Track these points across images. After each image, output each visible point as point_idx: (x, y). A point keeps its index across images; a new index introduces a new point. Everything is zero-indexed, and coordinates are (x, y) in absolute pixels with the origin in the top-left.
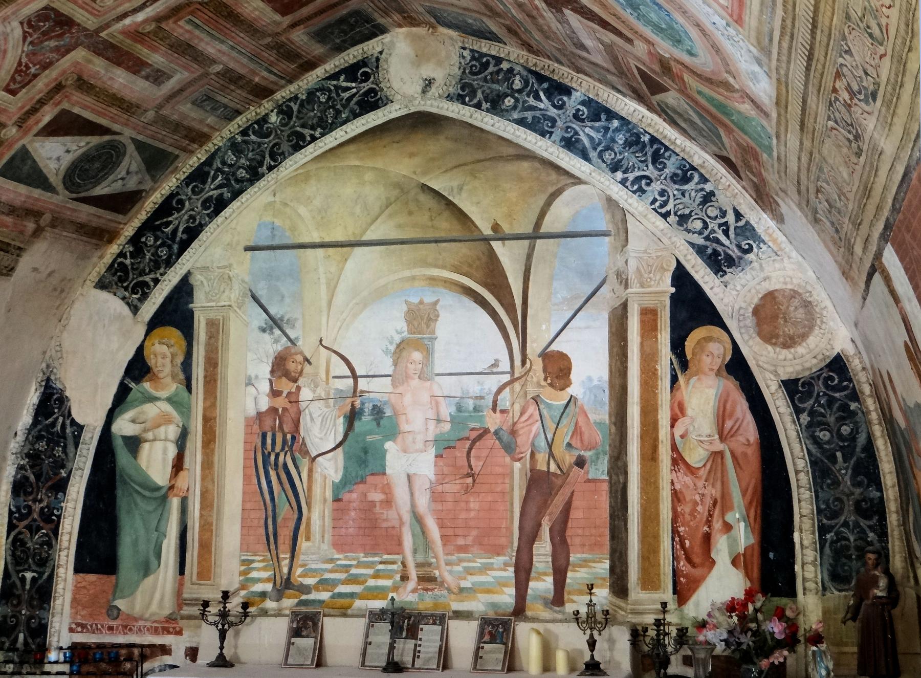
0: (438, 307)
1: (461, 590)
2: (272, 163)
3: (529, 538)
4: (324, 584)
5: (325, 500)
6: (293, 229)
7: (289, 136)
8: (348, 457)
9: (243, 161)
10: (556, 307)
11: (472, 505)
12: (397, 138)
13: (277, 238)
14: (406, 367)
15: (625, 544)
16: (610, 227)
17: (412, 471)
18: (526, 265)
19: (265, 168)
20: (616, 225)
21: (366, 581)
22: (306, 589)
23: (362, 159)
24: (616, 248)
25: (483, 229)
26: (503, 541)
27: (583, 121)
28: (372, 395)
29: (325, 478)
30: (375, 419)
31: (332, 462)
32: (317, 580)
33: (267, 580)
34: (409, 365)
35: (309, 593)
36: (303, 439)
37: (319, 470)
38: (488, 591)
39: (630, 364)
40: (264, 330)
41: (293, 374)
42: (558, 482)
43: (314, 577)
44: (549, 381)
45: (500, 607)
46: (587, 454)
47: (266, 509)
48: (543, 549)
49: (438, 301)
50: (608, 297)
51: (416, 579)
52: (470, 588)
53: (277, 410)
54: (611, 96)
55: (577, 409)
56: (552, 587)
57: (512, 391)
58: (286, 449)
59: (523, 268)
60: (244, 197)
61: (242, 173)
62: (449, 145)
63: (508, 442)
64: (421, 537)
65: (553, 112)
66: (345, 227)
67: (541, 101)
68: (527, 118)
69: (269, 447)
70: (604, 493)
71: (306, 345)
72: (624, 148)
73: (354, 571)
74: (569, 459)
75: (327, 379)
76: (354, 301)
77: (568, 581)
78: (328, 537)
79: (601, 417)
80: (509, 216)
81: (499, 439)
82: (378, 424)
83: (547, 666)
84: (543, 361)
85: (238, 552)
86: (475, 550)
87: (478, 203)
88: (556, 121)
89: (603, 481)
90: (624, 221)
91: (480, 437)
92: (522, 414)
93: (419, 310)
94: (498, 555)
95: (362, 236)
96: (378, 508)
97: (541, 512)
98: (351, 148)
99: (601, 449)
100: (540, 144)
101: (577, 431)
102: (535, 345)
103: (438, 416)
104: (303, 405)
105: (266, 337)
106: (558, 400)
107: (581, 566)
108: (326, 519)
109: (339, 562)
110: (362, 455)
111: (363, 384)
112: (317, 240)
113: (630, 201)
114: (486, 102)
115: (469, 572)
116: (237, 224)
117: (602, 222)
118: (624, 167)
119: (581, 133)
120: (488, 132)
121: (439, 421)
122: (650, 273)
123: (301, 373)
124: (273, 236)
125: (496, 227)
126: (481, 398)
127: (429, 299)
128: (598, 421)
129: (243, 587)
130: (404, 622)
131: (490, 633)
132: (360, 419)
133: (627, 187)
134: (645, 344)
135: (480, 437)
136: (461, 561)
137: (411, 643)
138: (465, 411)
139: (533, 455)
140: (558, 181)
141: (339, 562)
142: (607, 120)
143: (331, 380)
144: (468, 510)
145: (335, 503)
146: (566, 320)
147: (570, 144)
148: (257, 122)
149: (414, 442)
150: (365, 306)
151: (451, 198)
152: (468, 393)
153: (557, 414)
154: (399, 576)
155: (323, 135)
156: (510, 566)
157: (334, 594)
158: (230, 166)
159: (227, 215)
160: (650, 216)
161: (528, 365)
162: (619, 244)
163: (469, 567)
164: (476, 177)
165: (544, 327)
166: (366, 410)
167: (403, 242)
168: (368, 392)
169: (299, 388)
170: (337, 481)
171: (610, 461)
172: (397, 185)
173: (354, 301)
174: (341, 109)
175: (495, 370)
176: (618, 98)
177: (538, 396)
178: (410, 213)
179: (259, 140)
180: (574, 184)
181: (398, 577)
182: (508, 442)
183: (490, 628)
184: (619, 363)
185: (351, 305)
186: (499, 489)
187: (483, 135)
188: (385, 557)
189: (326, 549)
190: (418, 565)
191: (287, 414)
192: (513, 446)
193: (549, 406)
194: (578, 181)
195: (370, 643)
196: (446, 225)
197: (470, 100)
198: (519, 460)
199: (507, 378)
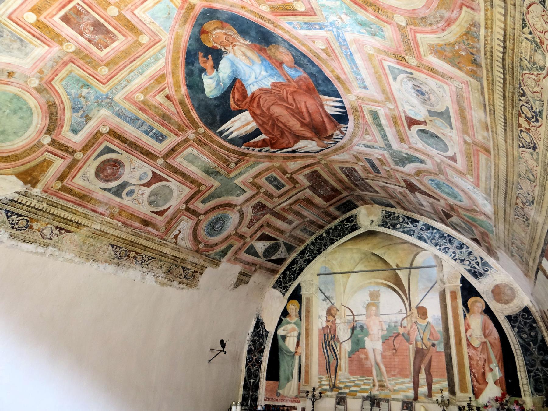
1: (395, 390)
6: (332, 268)
8: (352, 343)
26: (408, 373)
33: (327, 385)
35: (341, 390)
38: (404, 391)
42: (426, 352)
48: (423, 376)
50: (438, 288)
57: (407, 320)
60: (316, 259)
61: (315, 252)
62: (380, 240)
63: (407, 338)
65: (413, 228)
71: (337, 305)
73: (356, 382)
74: (429, 344)
78: (347, 370)
80: (402, 262)
81: (404, 337)
90: (441, 262)
92: (411, 328)
98: (349, 242)
101: (431, 334)
104: (337, 325)
106: (424, 323)
111: (356, 318)
115: (397, 384)
117: (434, 263)
121: (383, 330)
125: (397, 266)
126: (396, 322)
129: (320, 387)
139: (416, 342)
144: (395, 362)
147: (420, 238)
153: (424, 328)
155: (340, 239)
169: (335, 319)
181: (372, 385)
189: (347, 374)
190: (379, 381)
193: (420, 325)
194: (424, 250)
196: (380, 265)
199: (405, 315)
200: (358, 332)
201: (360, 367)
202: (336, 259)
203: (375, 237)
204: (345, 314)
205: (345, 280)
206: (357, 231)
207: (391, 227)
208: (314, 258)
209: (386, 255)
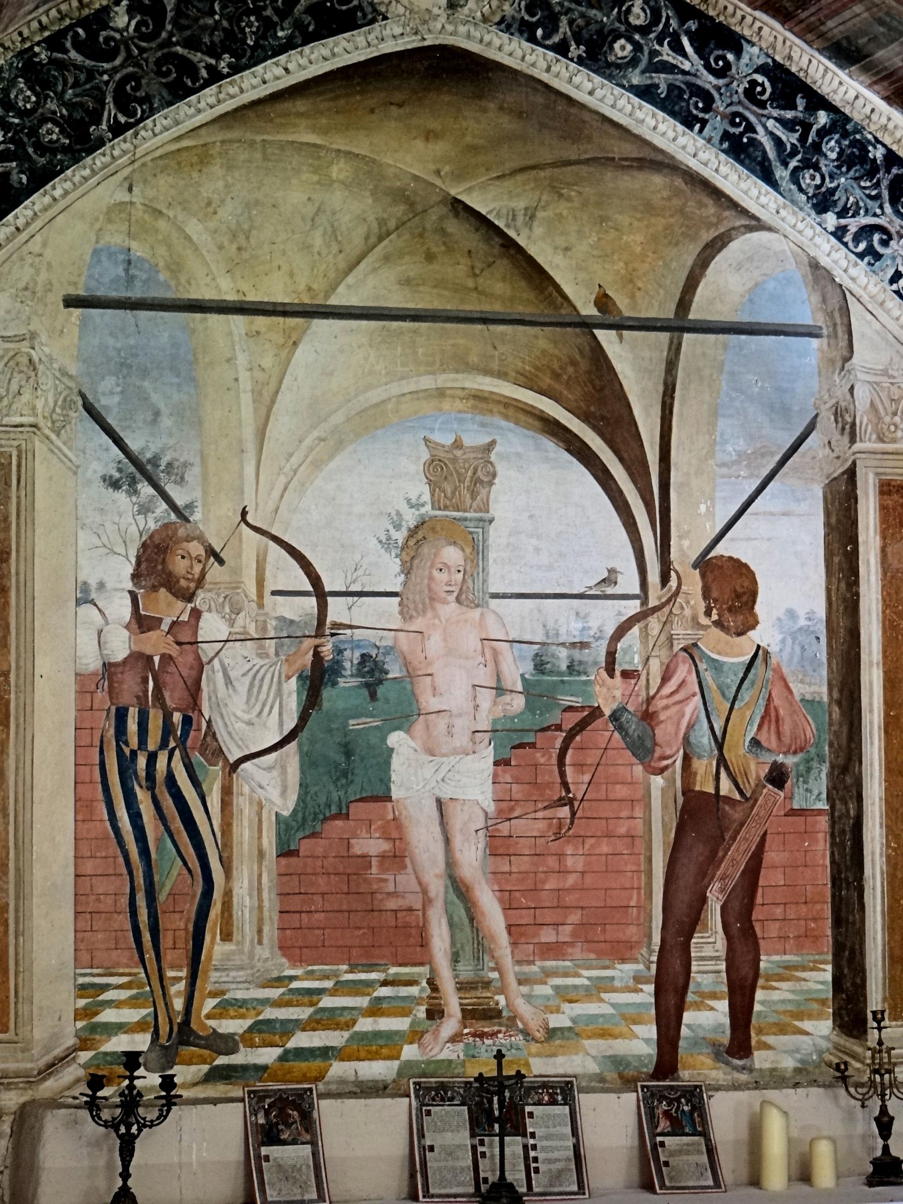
0: (493, 457)
1: (551, 1033)
2: (122, 119)
3: (682, 925)
4: (265, 1031)
5: (261, 854)
6: (176, 267)
7: (159, 63)
8: (308, 762)
9: (52, 105)
10: (724, 470)
11: (569, 862)
12: (398, 97)
13: (138, 284)
14: (431, 578)
15: (861, 933)
16: (820, 320)
17: (446, 793)
18: (666, 384)
19: (104, 126)
20: (831, 315)
21: (354, 1022)
22: (228, 1044)
23: (324, 131)
24: (832, 361)
25: (578, 305)
26: (632, 932)
27: (762, 105)
28: (358, 634)
29: (261, 806)
30: (367, 685)
31: (275, 773)
32: (248, 1022)
33: (140, 1027)
34: (436, 573)
35: (233, 1051)
36: (209, 722)
37: (246, 789)
38: (604, 1034)
39: (863, 589)
40: (115, 485)
41: (183, 583)
42: (736, 815)
43: (243, 1017)
44: (715, 617)
45: (628, 1064)
46: (790, 761)
47: (131, 873)
48: (710, 946)
49: (493, 443)
50: (821, 454)
51: (459, 1015)
52: (570, 1029)
53: (150, 659)
54: (814, 62)
55: (770, 674)
56: (727, 1021)
57: (645, 632)
58: (172, 744)
59: (661, 389)
60: (58, 187)
61: (51, 133)
62: (507, 123)
63: (639, 733)
64: (468, 929)
65: (708, 81)
66: (291, 275)
67: (685, 55)
68: (657, 86)
69: (134, 741)
70: (821, 836)
71: (212, 522)
72: (839, 167)
73: (327, 1002)
74: (757, 769)
75: (260, 595)
76: (315, 434)
77: (757, 1007)
78: (270, 931)
79: (813, 688)
80: (629, 281)
81: (620, 728)
82: (373, 696)
83: (803, 1173)
84: (703, 576)
85: (70, 970)
86: (577, 951)
87: (567, 249)
88: (712, 100)
89: (820, 812)
90: (845, 311)
91: (582, 726)
92: (665, 679)
93: (455, 460)
94: (623, 960)
95: (327, 297)
96: (374, 870)
97: (704, 876)
98: (301, 105)
99: (813, 751)
100: (682, 140)
101: (770, 716)
102: (686, 543)
103: (499, 679)
104: (207, 651)
105: (122, 497)
106: (734, 653)
107: (781, 979)
108: (265, 895)
109: (295, 985)
110: (341, 759)
111: (337, 610)
112: (231, 297)
113: (853, 271)
114: (578, 45)
115: (566, 995)
116: (44, 245)
117: (804, 309)
118: (841, 204)
119: (759, 129)
120: (583, 106)
121: (500, 690)
122: (895, 414)
123: (200, 581)
124: (130, 279)
125: (603, 301)
126: (583, 645)
127: (474, 438)
128: (808, 697)
129: (84, 1044)
130: (491, 1102)
131: (667, 1114)
132: (334, 684)
133: (846, 245)
134: (889, 549)
135: (582, 726)
136: (548, 974)
137: (514, 1145)
138: (551, 673)
139: (687, 759)
140: (720, 220)
141: (295, 985)
142: (807, 109)
143: (268, 599)
144: (563, 872)
145: (284, 861)
146: (745, 497)
147: (740, 148)
148: (82, 22)
149: (450, 734)
150: (340, 445)
151: (511, 233)
152: (557, 635)
153: (732, 681)
154: (423, 1008)
155: (236, 69)
156: (647, 982)
157: (287, 1052)
158: (22, 113)
159: (21, 222)
160: (890, 304)
161: (673, 583)
162: (837, 355)
163: (566, 987)
164: (561, 195)
165: (703, 508)
166: (347, 665)
167: (416, 316)
168: (351, 627)
169: (196, 614)
170: (286, 813)
171: (830, 775)
172: (400, 196)
173: (315, 434)
174: (275, 19)
175: (610, 591)
176: (826, 69)
177: (695, 645)
178: (430, 257)
179: (88, 62)
180: (751, 229)
181: (421, 1012)
182: (639, 733)
183: (664, 1106)
184: (843, 585)
185: (308, 441)
186: (622, 830)
187: (573, 111)
188: (393, 970)
189: (268, 957)
190: (462, 987)
191: (172, 669)
192: (648, 744)
193: (717, 666)
194: (757, 225)
195: (432, 1148)
196: (501, 289)
197: (546, 36)
198: (661, 771)
199: (634, 607)
200: (345, 699)
201: (348, 908)
202: (209, 209)
203: (480, 97)
204: (260, 583)
205: (268, 361)
206: (359, 37)
207: (575, 50)
208: (41, 178)
209: (539, 230)
